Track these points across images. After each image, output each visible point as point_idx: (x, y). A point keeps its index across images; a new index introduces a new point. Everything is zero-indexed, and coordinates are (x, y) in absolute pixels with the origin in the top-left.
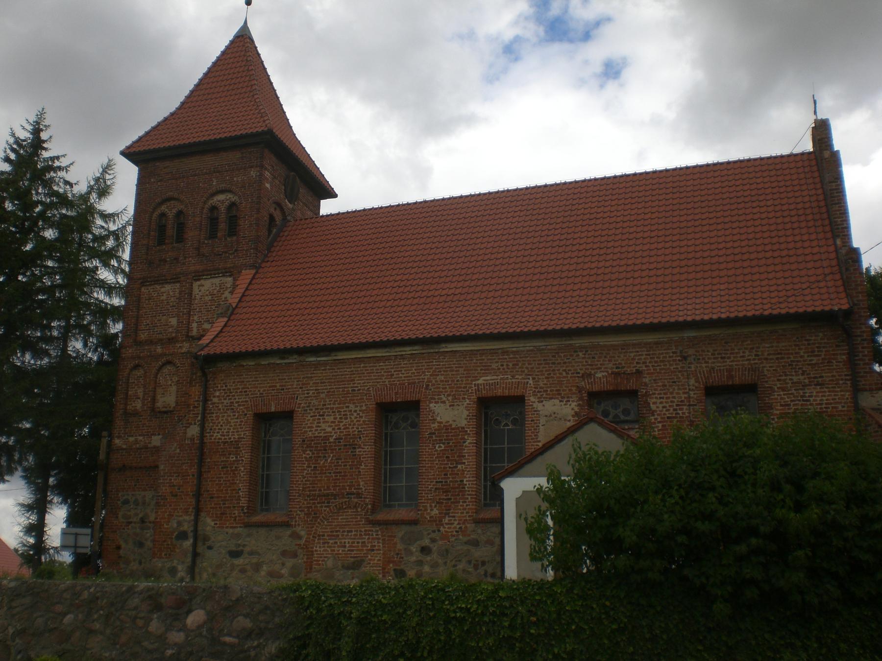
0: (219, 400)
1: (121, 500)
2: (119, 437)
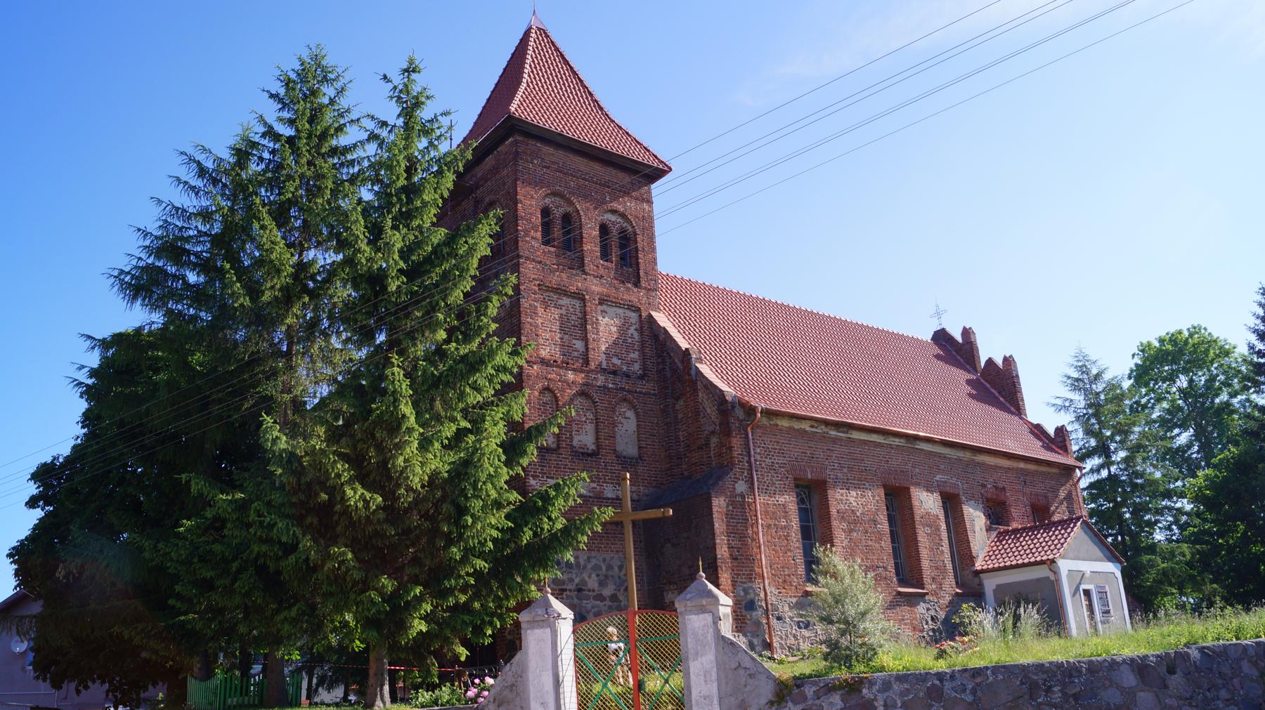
0: (761, 457)
2: (535, 477)
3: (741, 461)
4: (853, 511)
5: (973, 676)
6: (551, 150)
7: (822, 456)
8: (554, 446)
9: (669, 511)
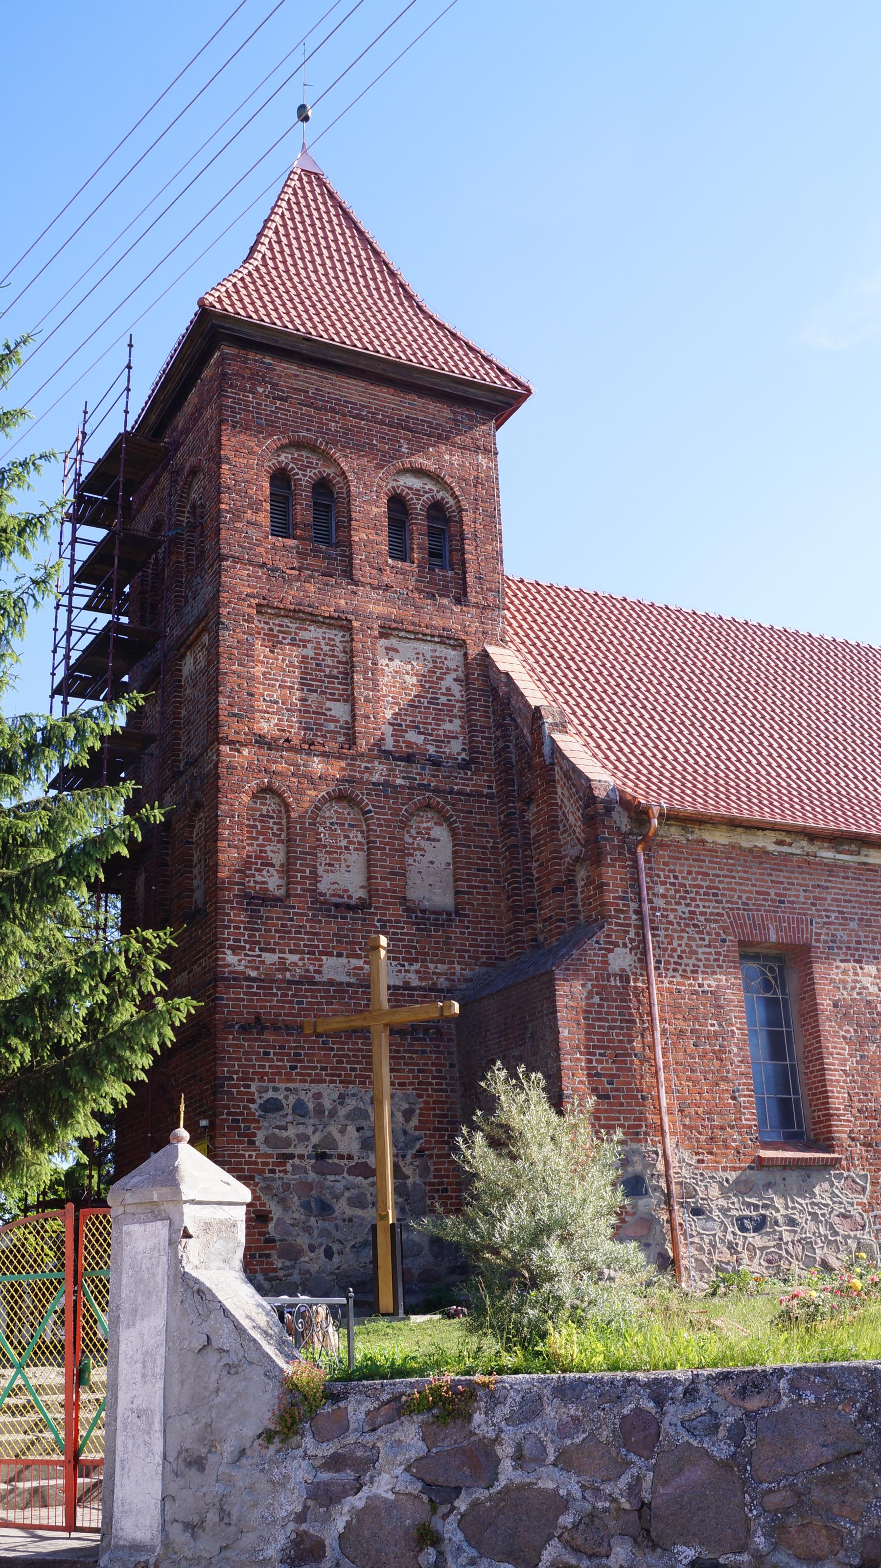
0: (667, 903)
1: (259, 1101)
2: (235, 949)
3: (622, 912)
4: (868, 1002)
5: (743, 1393)
6: (292, 368)
7: (802, 899)
8: (281, 893)
9: (451, 1006)
